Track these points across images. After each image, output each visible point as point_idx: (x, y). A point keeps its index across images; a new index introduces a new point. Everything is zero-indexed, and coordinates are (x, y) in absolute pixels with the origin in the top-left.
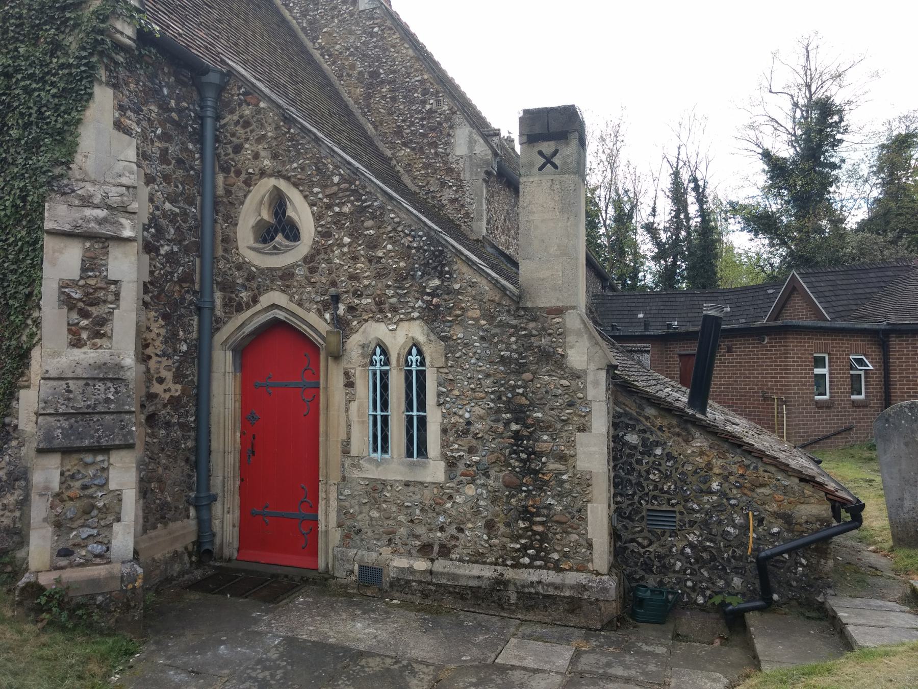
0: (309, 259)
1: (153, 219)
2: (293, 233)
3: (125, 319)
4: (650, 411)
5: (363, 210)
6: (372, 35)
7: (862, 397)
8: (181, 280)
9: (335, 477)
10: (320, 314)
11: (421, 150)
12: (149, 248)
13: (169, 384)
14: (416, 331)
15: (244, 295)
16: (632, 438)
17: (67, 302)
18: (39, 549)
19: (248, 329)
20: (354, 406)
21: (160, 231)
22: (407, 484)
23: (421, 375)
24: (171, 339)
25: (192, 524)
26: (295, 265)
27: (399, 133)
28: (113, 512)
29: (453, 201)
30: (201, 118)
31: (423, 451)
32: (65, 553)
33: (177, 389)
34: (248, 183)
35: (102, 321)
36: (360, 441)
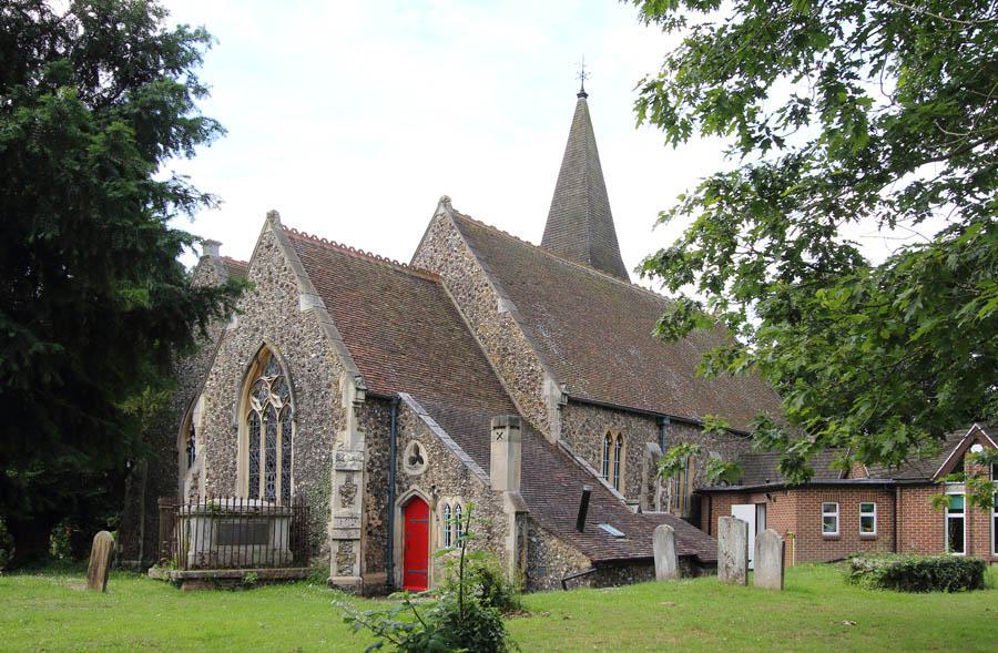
0: (426, 472)
1: (371, 460)
2: (422, 462)
3: (358, 498)
6: (504, 327)
7: (874, 533)
8: (382, 480)
12: (369, 471)
13: (377, 520)
14: (458, 499)
15: (405, 486)
16: (534, 539)
17: (341, 493)
18: (333, 568)
21: (373, 464)
24: (378, 503)
25: (386, 575)
27: (516, 383)
28: (353, 560)
29: (542, 421)
30: (390, 417)
32: (340, 571)
33: (380, 523)
34: (407, 441)
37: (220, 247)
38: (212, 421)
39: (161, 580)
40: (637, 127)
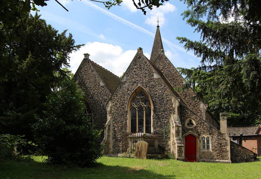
2: (192, 124)
4: (234, 144)
5: (202, 122)
9: (198, 152)
10: (196, 133)
11: (194, 107)
15: (186, 131)
16: (233, 147)
19: (187, 135)
20: (201, 144)
22: (207, 152)
23: (209, 140)
26: (193, 128)
31: (209, 149)
34: (187, 118)
35: (179, 134)
36: (202, 147)
37: (89, 56)
38: (115, 109)
39: (127, 157)
40: (83, 45)
